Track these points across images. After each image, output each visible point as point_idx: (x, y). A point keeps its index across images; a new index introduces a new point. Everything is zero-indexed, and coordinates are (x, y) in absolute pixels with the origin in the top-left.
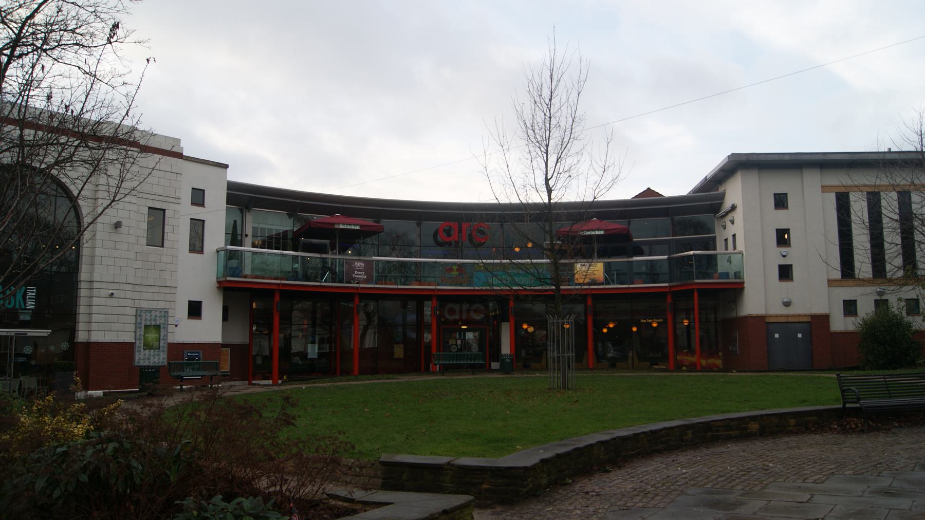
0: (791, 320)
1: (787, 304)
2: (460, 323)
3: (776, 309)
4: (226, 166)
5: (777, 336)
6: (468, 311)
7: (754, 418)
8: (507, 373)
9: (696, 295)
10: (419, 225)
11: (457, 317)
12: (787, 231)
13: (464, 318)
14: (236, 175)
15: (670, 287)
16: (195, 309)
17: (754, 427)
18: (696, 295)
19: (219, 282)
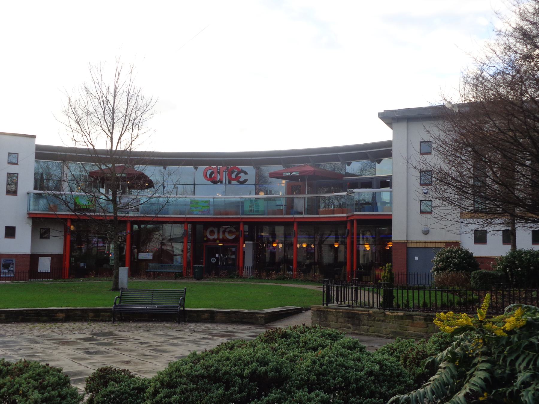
0: (428, 245)
1: (426, 233)
2: (218, 241)
3: (416, 237)
4: (34, 137)
5: (417, 258)
6: (224, 232)
7: (62, 311)
8: (198, 279)
9: (295, 224)
10: (165, 168)
11: (216, 236)
12: (9, 192)
13: (221, 237)
14: (39, 141)
15: (348, 217)
16: (10, 232)
17: (61, 315)
18: (295, 224)
19: (29, 214)
